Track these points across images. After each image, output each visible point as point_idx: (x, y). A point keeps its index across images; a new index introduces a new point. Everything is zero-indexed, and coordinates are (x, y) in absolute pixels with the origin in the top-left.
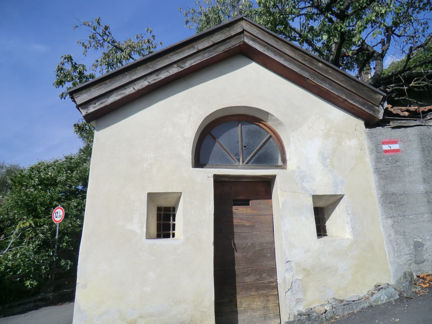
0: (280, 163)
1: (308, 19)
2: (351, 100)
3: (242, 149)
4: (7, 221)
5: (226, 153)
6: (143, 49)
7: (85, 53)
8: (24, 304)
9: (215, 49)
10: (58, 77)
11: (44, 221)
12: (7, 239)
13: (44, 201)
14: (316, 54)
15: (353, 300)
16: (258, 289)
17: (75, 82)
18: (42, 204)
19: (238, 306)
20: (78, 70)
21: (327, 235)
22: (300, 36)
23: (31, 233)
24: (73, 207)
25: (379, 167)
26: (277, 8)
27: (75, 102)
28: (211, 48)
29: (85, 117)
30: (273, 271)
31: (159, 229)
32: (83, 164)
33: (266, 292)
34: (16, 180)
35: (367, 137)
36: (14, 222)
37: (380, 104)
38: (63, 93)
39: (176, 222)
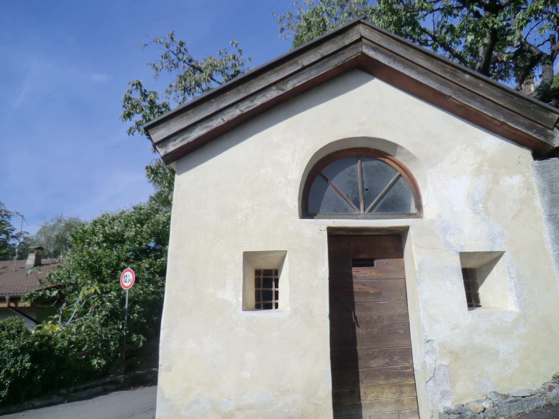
0: (413, 210)
1: (445, 15)
2: (513, 122)
3: (363, 191)
4: (68, 286)
5: (343, 199)
6: (227, 68)
7: (157, 77)
8: (91, 387)
9: (324, 64)
10: (124, 109)
11: (111, 286)
12: (69, 308)
13: (110, 262)
14: (456, 61)
15: (524, 395)
16: (388, 375)
17: (151, 117)
18: (107, 266)
19: (362, 398)
20: (149, 99)
21: (480, 306)
22: (434, 38)
23: (96, 301)
24: (144, 269)
25: (554, 213)
26: (401, 3)
27: (150, 138)
28: (319, 64)
29: (164, 158)
30: (407, 353)
31: (257, 298)
32: (155, 216)
33: (399, 381)
34: (78, 236)
35: (536, 172)
36: (77, 288)
37: (555, 126)
38: (131, 128)
39: (280, 289)
